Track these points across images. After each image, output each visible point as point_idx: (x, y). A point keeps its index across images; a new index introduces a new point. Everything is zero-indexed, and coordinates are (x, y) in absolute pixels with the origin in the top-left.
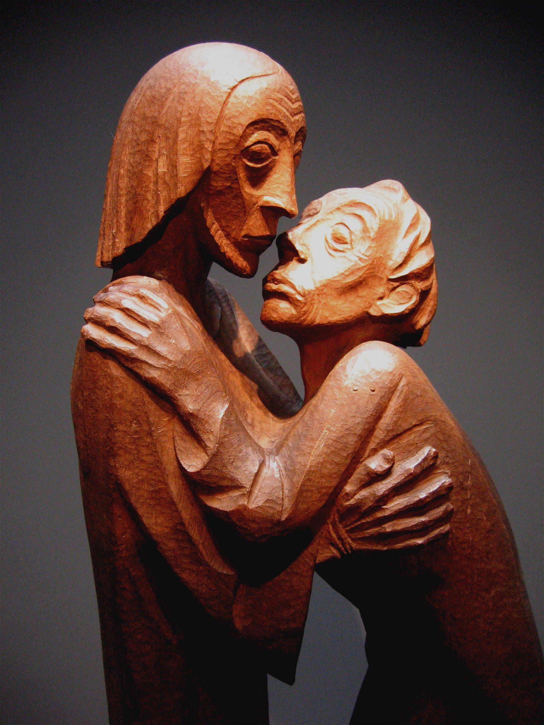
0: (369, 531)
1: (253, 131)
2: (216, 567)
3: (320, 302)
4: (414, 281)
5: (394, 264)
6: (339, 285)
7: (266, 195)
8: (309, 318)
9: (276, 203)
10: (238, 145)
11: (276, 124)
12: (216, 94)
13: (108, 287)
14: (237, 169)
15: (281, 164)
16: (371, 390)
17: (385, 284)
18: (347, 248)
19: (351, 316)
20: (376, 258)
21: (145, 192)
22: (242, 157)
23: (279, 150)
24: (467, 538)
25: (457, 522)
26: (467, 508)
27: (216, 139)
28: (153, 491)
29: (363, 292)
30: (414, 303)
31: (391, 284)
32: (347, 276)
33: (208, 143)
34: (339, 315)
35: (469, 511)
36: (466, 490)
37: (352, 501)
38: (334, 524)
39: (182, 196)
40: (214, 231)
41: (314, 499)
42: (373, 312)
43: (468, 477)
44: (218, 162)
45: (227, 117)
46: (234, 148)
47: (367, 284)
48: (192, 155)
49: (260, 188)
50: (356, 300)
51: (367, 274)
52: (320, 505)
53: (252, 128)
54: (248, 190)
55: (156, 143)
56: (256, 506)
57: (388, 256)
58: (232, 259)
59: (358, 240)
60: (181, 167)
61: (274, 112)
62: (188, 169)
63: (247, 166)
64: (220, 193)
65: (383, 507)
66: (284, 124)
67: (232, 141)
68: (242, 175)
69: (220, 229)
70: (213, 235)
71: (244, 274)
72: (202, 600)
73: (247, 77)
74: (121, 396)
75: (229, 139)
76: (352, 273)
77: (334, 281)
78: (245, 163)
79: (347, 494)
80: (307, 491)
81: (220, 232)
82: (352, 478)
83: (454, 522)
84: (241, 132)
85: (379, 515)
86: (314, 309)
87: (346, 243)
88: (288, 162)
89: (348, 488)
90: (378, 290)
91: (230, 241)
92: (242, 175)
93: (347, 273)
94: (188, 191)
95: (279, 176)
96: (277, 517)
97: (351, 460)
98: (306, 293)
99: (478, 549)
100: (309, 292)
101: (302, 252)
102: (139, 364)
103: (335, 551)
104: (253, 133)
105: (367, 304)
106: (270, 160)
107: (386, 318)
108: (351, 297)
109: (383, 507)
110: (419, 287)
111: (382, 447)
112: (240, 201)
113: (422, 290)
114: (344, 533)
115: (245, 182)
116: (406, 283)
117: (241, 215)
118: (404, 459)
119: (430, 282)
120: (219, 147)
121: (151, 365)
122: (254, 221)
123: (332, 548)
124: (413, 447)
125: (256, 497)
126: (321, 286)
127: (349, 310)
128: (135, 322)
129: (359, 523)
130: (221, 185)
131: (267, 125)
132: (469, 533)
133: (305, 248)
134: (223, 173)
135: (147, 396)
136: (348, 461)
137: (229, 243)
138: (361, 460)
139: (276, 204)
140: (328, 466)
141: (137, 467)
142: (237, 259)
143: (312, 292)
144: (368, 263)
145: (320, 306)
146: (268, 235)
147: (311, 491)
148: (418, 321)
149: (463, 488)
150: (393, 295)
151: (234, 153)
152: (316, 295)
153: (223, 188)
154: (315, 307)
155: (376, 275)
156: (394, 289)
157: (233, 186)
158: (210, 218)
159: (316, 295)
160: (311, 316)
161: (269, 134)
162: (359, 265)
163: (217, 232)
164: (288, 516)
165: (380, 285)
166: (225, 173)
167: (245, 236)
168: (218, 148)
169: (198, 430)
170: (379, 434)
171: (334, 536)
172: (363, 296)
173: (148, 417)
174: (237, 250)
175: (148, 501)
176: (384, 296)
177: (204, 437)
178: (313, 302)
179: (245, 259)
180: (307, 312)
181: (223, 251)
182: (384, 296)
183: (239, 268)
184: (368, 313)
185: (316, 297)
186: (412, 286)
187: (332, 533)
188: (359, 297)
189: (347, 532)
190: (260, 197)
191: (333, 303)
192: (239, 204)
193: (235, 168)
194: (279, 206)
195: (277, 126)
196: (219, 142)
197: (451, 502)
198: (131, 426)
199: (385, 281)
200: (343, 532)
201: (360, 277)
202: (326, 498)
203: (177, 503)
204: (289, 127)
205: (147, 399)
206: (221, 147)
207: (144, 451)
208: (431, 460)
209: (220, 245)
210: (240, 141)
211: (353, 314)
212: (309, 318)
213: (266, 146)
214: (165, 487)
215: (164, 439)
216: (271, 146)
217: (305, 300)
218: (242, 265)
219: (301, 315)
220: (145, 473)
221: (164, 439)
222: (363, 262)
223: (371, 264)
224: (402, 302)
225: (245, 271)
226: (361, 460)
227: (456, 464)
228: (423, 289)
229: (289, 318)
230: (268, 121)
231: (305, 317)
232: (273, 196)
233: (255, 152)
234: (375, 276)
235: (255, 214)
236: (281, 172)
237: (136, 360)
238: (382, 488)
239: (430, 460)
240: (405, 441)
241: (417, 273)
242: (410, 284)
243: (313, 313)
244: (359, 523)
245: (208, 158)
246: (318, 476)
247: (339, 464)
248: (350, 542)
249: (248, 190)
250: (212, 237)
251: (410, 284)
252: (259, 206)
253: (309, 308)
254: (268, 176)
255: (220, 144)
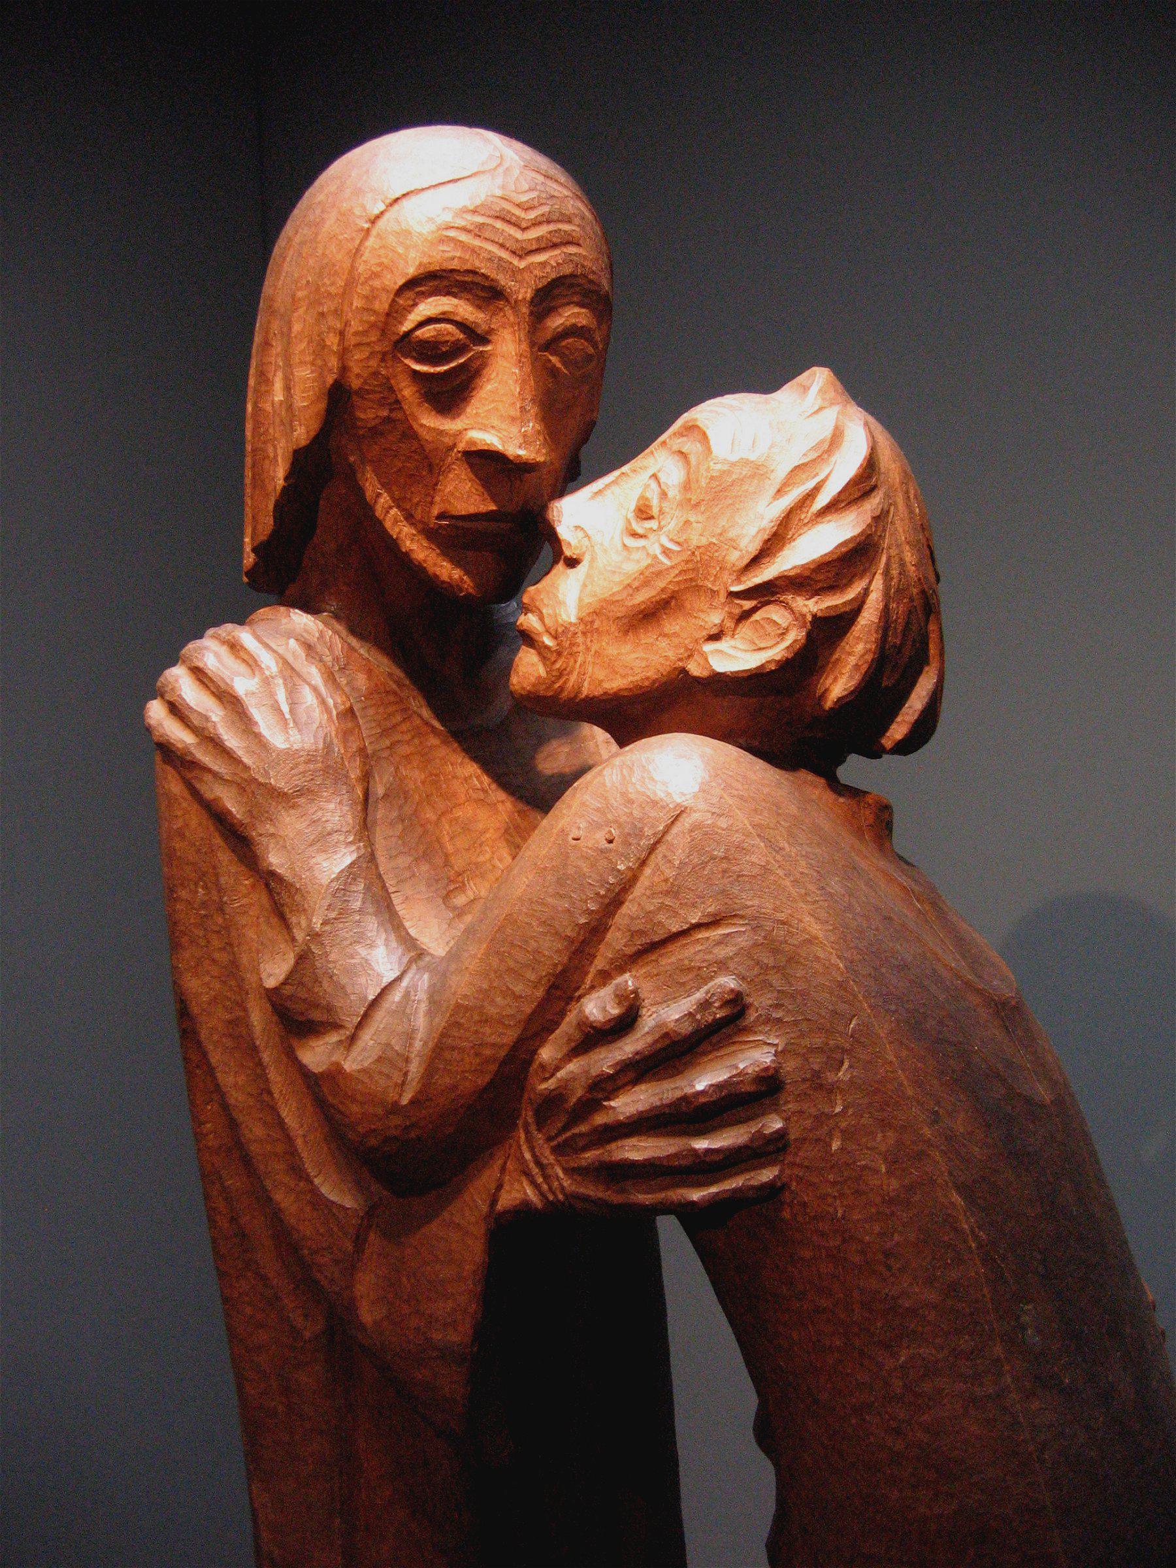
0: (588, 1155)
1: (414, 300)
2: (324, 1190)
3: (588, 649)
4: (792, 596)
5: (741, 557)
6: (620, 611)
7: (472, 428)
8: (570, 684)
9: (489, 442)
10: (383, 331)
11: (468, 279)
12: (346, 236)
13: (586, 638)
14: (392, 382)
15: (499, 359)
16: (606, 839)
17: (724, 604)
18: (651, 529)
19: (647, 678)
20: (699, 547)
21: (265, 442)
22: (399, 355)
23: (491, 331)
24: (831, 1210)
25: (800, 1166)
26: (830, 1134)
27: (346, 325)
28: (229, 1022)
29: (672, 625)
30: (791, 645)
31: (738, 604)
32: (637, 589)
33: (331, 335)
34: (623, 677)
35: (835, 1145)
36: (830, 1091)
37: (551, 1084)
38: (526, 1127)
39: (300, 446)
40: (382, 511)
41: (467, 1067)
42: (695, 669)
43: (842, 1063)
44: (356, 370)
45: (362, 279)
46: (380, 340)
47: (680, 607)
48: (313, 364)
49: (459, 415)
50: (658, 643)
51: (678, 583)
52: (483, 1080)
53: (410, 294)
54: (429, 421)
55: (272, 346)
56: (359, 1067)
57: (731, 540)
58: (425, 565)
59: (672, 508)
60: (297, 388)
61: (458, 254)
62: (309, 391)
63: (415, 372)
64: (375, 432)
65: (605, 1103)
66: (489, 276)
67: (373, 325)
68: (408, 392)
69: (393, 504)
70: (381, 518)
71: (462, 595)
72: (306, 1252)
73: (405, 192)
74: (182, 835)
75: (368, 322)
76: (646, 583)
77: (613, 602)
78: (409, 367)
79: (542, 1067)
80: (453, 1048)
81: (394, 511)
82: (557, 1032)
83: (793, 1164)
84: (386, 306)
85: (600, 1119)
86: (578, 664)
87: (652, 518)
88: (513, 353)
89: (546, 1054)
90: (706, 619)
91: (416, 527)
92: (408, 392)
93: (636, 584)
94: (313, 434)
95: (496, 385)
96: (392, 1095)
97: (548, 991)
98: (560, 630)
99: (861, 1241)
100: (566, 630)
101: (569, 544)
102: (197, 772)
103: (530, 1191)
104: (415, 305)
105: (682, 651)
106: (469, 355)
107: (720, 683)
108: (648, 637)
109: (605, 1103)
110: (805, 610)
111: (622, 970)
112: (415, 445)
113: (814, 616)
114: (547, 1152)
115: (419, 405)
116: (774, 601)
117: (424, 473)
118: (668, 1000)
119: (851, 594)
120: (352, 340)
121: (216, 775)
122: (454, 484)
123: (525, 1183)
124: (690, 976)
125: (364, 1049)
126: (589, 614)
127: (644, 664)
128: (208, 692)
129: (569, 1134)
130: (372, 416)
131: (446, 283)
132: (835, 1197)
133: (580, 534)
134: (368, 392)
135: (217, 834)
136: (540, 993)
137: (414, 532)
138: (577, 994)
139: (489, 445)
140: (499, 1000)
141: (208, 972)
142: (435, 565)
143: (572, 629)
144: (679, 559)
145: (589, 659)
146: (492, 511)
147: (462, 1050)
148: (826, 690)
149: (817, 1084)
150: (745, 629)
151: (380, 349)
152: (579, 635)
153: (377, 421)
154: (580, 659)
155: (702, 586)
156: (745, 615)
157: (393, 415)
158: (371, 484)
159: (579, 635)
160: (573, 678)
161: (455, 301)
162: (662, 563)
163: (388, 512)
164: (413, 1097)
165: (711, 607)
166: (376, 392)
167: (441, 516)
168: (352, 343)
169: (283, 905)
170: (616, 940)
171: (528, 1156)
172: (674, 633)
173: (217, 875)
174: (434, 547)
175: (224, 1040)
176: (722, 631)
177: (293, 920)
178: (575, 649)
179: (457, 562)
180: (566, 672)
181: (404, 550)
182: (722, 631)
183: (443, 582)
184: (684, 671)
185: (580, 639)
186: (787, 606)
187: (524, 1147)
188: (665, 635)
189: (556, 1150)
190: (460, 433)
191: (612, 651)
192: (415, 452)
193: (388, 379)
194: (493, 448)
195: (473, 283)
196: (352, 330)
197: (784, 1115)
198: (197, 892)
199: (722, 597)
200: (549, 1158)
201: (663, 590)
202: (493, 1068)
203: (261, 1048)
204: (503, 280)
205: (218, 841)
206: (358, 339)
207: (216, 942)
208: (720, 1007)
209: (397, 538)
210: (386, 323)
211: (651, 674)
212: (570, 684)
213: (449, 327)
214: (242, 1014)
215: (243, 920)
216: (462, 326)
217: (558, 645)
218: (450, 577)
219: (553, 679)
220: (218, 986)
221: (243, 920)
222: (670, 558)
223: (687, 562)
224: (762, 645)
225: (461, 590)
226: (577, 994)
227: (804, 1026)
228: (819, 614)
229: (534, 685)
230: (444, 274)
231: (561, 682)
232: (483, 428)
233: (424, 343)
234: (698, 588)
235: (455, 469)
236: (500, 377)
237: (194, 765)
238: (606, 1060)
239: (717, 1008)
240: (673, 959)
241: (798, 576)
242: (781, 602)
243: (576, 673)
244: (569, 1134)
245: (333, 366)
246: (476, 1018)
247: (521, 997)
248: (561, 1175)
249: (429, 421)
250: (380, 523)
251: (781, 602)
252: (459, 452)
253: (568, 664)
254: (473, 389)
255: (356, 334)
